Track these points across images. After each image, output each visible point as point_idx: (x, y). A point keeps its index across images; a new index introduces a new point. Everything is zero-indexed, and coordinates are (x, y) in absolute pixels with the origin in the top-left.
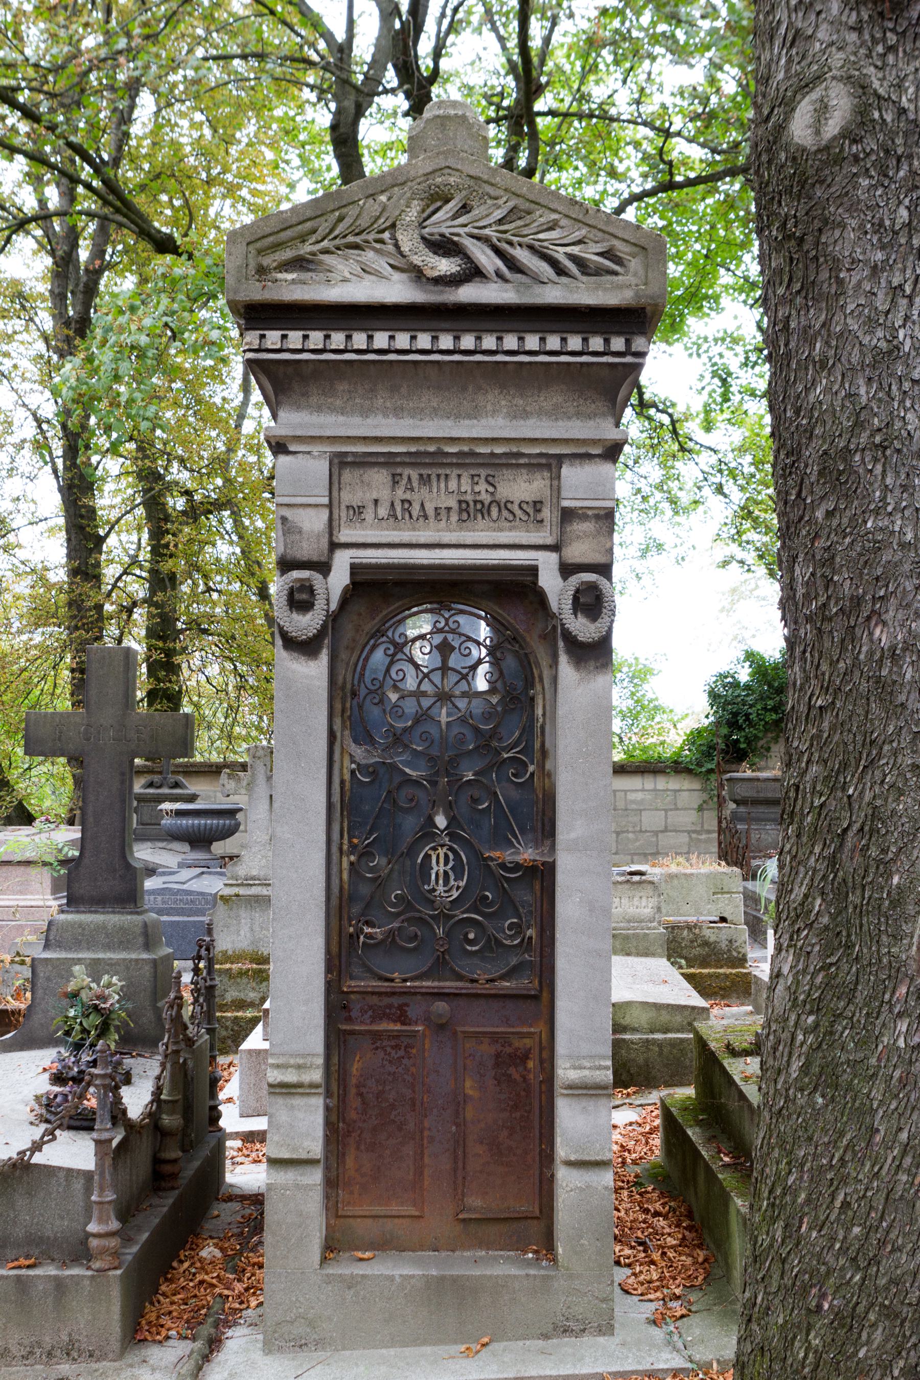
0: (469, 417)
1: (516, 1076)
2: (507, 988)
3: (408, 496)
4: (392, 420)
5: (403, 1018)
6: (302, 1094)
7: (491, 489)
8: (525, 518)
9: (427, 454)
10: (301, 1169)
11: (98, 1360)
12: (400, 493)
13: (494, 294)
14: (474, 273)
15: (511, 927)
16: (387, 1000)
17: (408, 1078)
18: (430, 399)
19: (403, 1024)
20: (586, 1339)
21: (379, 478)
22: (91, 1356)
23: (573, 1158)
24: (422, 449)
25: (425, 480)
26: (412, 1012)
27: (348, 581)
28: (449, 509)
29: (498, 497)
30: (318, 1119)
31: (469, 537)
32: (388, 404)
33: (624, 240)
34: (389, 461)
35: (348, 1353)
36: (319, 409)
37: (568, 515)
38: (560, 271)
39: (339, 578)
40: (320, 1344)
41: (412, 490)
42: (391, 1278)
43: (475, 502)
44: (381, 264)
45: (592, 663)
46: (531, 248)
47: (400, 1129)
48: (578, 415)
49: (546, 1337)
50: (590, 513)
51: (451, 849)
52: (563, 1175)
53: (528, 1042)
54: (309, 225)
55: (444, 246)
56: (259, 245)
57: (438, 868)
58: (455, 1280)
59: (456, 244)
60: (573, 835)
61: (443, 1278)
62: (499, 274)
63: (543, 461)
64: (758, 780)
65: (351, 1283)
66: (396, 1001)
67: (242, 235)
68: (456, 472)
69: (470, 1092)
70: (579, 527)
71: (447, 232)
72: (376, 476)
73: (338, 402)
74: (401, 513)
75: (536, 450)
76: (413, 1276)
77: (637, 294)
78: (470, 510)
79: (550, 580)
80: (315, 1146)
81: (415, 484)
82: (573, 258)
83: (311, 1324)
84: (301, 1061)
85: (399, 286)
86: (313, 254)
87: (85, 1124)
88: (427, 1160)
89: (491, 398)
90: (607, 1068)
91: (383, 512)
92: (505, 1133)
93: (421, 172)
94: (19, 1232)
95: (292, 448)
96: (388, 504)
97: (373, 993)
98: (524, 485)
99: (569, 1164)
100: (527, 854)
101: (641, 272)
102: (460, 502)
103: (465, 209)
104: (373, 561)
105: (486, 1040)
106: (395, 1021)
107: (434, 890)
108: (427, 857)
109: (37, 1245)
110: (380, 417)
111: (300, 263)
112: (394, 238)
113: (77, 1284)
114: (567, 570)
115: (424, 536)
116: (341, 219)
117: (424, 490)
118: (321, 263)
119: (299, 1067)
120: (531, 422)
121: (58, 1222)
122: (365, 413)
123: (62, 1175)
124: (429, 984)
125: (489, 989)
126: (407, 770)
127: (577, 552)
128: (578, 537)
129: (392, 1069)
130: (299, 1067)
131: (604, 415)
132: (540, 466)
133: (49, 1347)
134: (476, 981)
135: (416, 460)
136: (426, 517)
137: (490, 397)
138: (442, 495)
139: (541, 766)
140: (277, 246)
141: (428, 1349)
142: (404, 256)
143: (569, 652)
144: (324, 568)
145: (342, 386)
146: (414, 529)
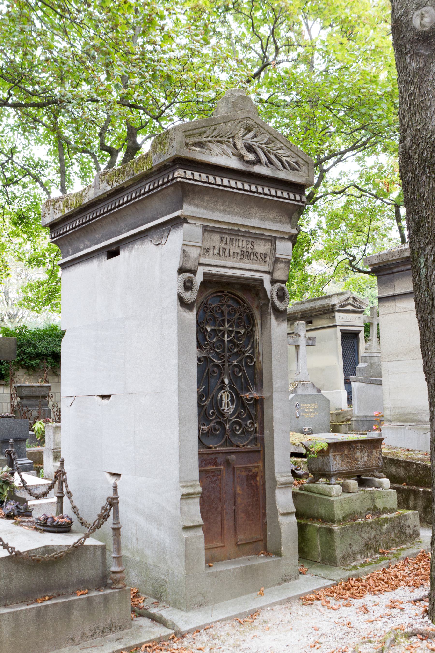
0: (247, 217)
1: (253, 484)
2: (249, 449)
3: (225, 247)
4: (222, 215)
5: (216, 464)
6: (192, 498)
7: (252, 247)
8: (261, 260)
9: (234, 230)
10: (195, 530)
11: (123, 630)
12: (223, 245)
13: (265, 171)
14: (258, 161)
15: (250, 423)
16: (210, 456)
17: (218, 488)
18: (235, 208)
19: (216, 466)
20: (292, 582)
21: (216, 237)
22: (120, 628)
23: (285, 512)
24: (233, 228)
25: (231, 241)
26: (219, 460)
27: (202, 280)
28: (238, 253)
29: (254, 251)
30: (198, 508)
31: (243, 266)
32: (221, 208)
33: (302, 159)
34: (221, 231)
35: (217, 605)
36: (198, 206)
37: (277, 260)
38: (284, 167)
39: (199, 279)
40: (207, 603)
41: (227, 244)
42: (230, 570)
43: (246, 251)
44: (229, 151)
45: (281, 319)
46: (275, 155)
47: (216, 510)
48: (280, 222)
49: (279, 584)
50: (283, 260)
51: (230, 392)
52: (281, 519)
53: (257, 469)
54: (204, 129)
55: (250, 148)
56: (186, 133)
57: (225, 400)
58: (251, 567)
59: (253, 149)
60: (277, 386)
61: (247, 567)
62: (266, 165)
63: (270, 238)
64: (33, 387)
65: (216, 575)
66: (213, 457)
67: (181, 128)
68: (242, 239)
69: (239, 492)
70: (280, 266)
71: (251, 143)
72: (216, 237)
73: (204, 204)
74: (222, 253)
75: (268, 234)
76: (237, 568)
77: (307, 181)
78: (245, 255)
79: (267, 285)
80: (199, 520)
81: (228, 242)
82: (287, 161)
83: (203, 596)
84: (192, 484)
85: (235, 161)
86: (205, 142)
87: (66, 529)
88: (225, 522)
89: (254, 211)
90: (289, 476)
91: (216, 252)
92: (251, 507)
93: (241, 117)
94: (73, 579)
95: (189, 221)
96: (218, 249)
97: (205, 454)
98: (263, 247)
99: (284, 514)
100: (255, 395)
101: (307, 172)
102: (242, 251)
103: (255, 136)
104: (211, 272)
105: (244, 470)
106: (213, 465)
107: (224, 410)
108: (222, 396)
109: (82, 584)
110: (218, 212)
111: (201, 145)
112: (233, 141)
113: (113, 596)
114: (273, 282)
115: (228, 263)
116: (215, 129)
117: (231, 245)
118: (208, 146)
119: (192, 486)
120: (267, 222)
121: (91, 572)
122: (214, 210)
123: (91, 549)
124: (223, 449)
125: (243, 449)
126: (215, 360)
127: (279, 275)
128: (279, 269)
129: (213, 485)
130: (192, 486)
131: (288, 223)
132: (268, 240)
133: (102, 628)
134: (239, 446)
135: (230, 232)
136: (230, 256)
137: (254, 210)
138: (235, 248)
139: (258, 358)
140: (192, 135)
141: (244, 597)
142: (236, 149)
143: (274, 314)
144: (194, 272)
145: (207, 198)
146: (225, 260)
